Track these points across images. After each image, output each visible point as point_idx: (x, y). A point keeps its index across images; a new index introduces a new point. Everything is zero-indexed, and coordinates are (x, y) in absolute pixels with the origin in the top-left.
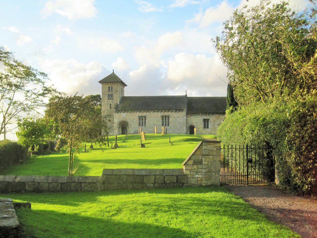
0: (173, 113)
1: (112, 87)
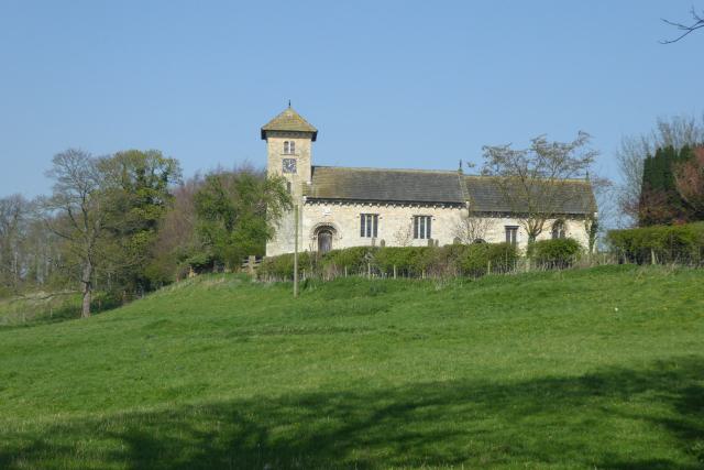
0: (440, 210)
1: (293, 144)
